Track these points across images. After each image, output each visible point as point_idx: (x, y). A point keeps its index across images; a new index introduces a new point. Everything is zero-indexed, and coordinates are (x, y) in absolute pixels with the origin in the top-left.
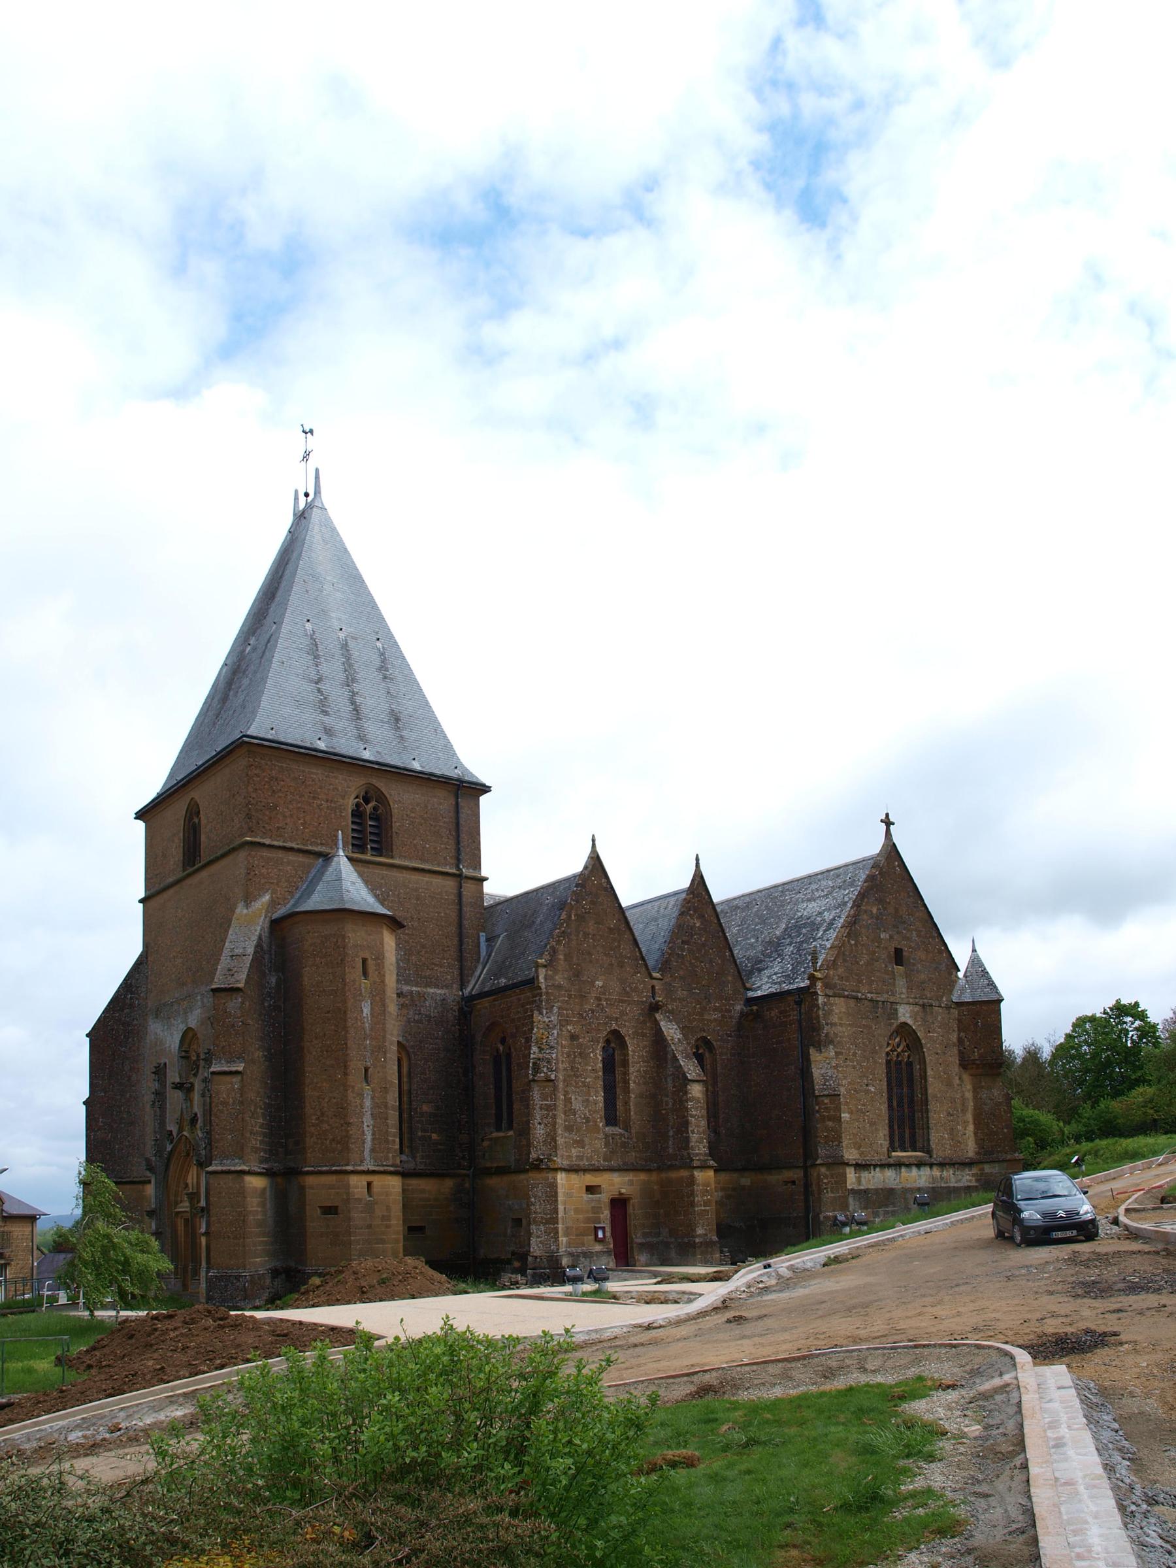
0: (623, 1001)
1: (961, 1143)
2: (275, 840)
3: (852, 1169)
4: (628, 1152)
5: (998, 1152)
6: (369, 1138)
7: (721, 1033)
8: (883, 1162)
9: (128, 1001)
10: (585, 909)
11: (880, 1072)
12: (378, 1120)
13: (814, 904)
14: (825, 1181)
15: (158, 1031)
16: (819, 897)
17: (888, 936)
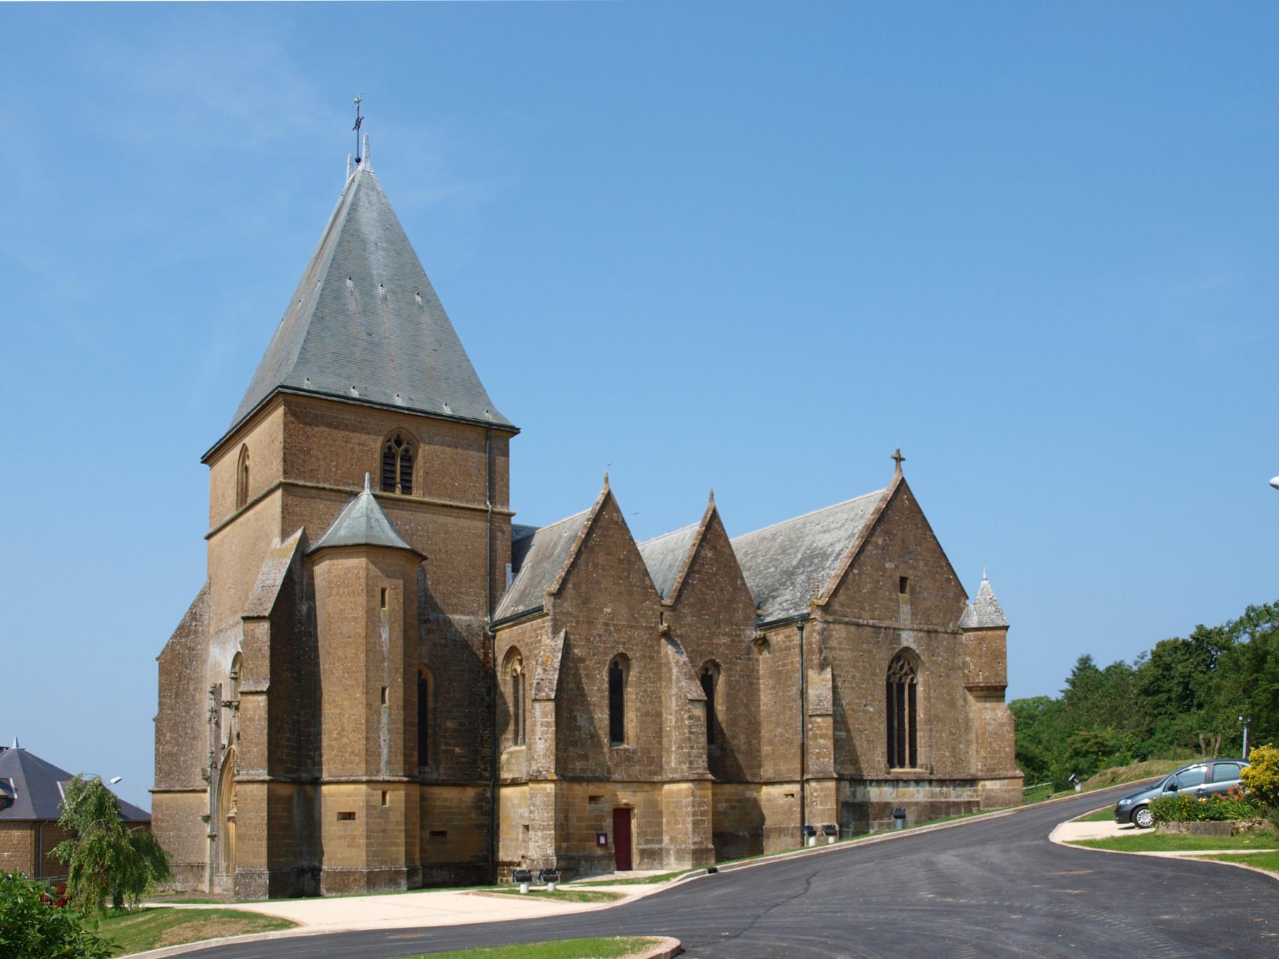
0: (632, 627)
1: (963, 761)
2: (309, 481)
3: (847, 784)
4: (632, 766)
5: (1000, 770)
6: (385, 751)
7: (730, 656)
8: (880, 778)
9: (193, 628)
10: (595, 541)
11: (880, 693)
12: (395, 735)
13: (828, 535)
15: (217, 655)
16: (834, 529)
17: (893, 566)
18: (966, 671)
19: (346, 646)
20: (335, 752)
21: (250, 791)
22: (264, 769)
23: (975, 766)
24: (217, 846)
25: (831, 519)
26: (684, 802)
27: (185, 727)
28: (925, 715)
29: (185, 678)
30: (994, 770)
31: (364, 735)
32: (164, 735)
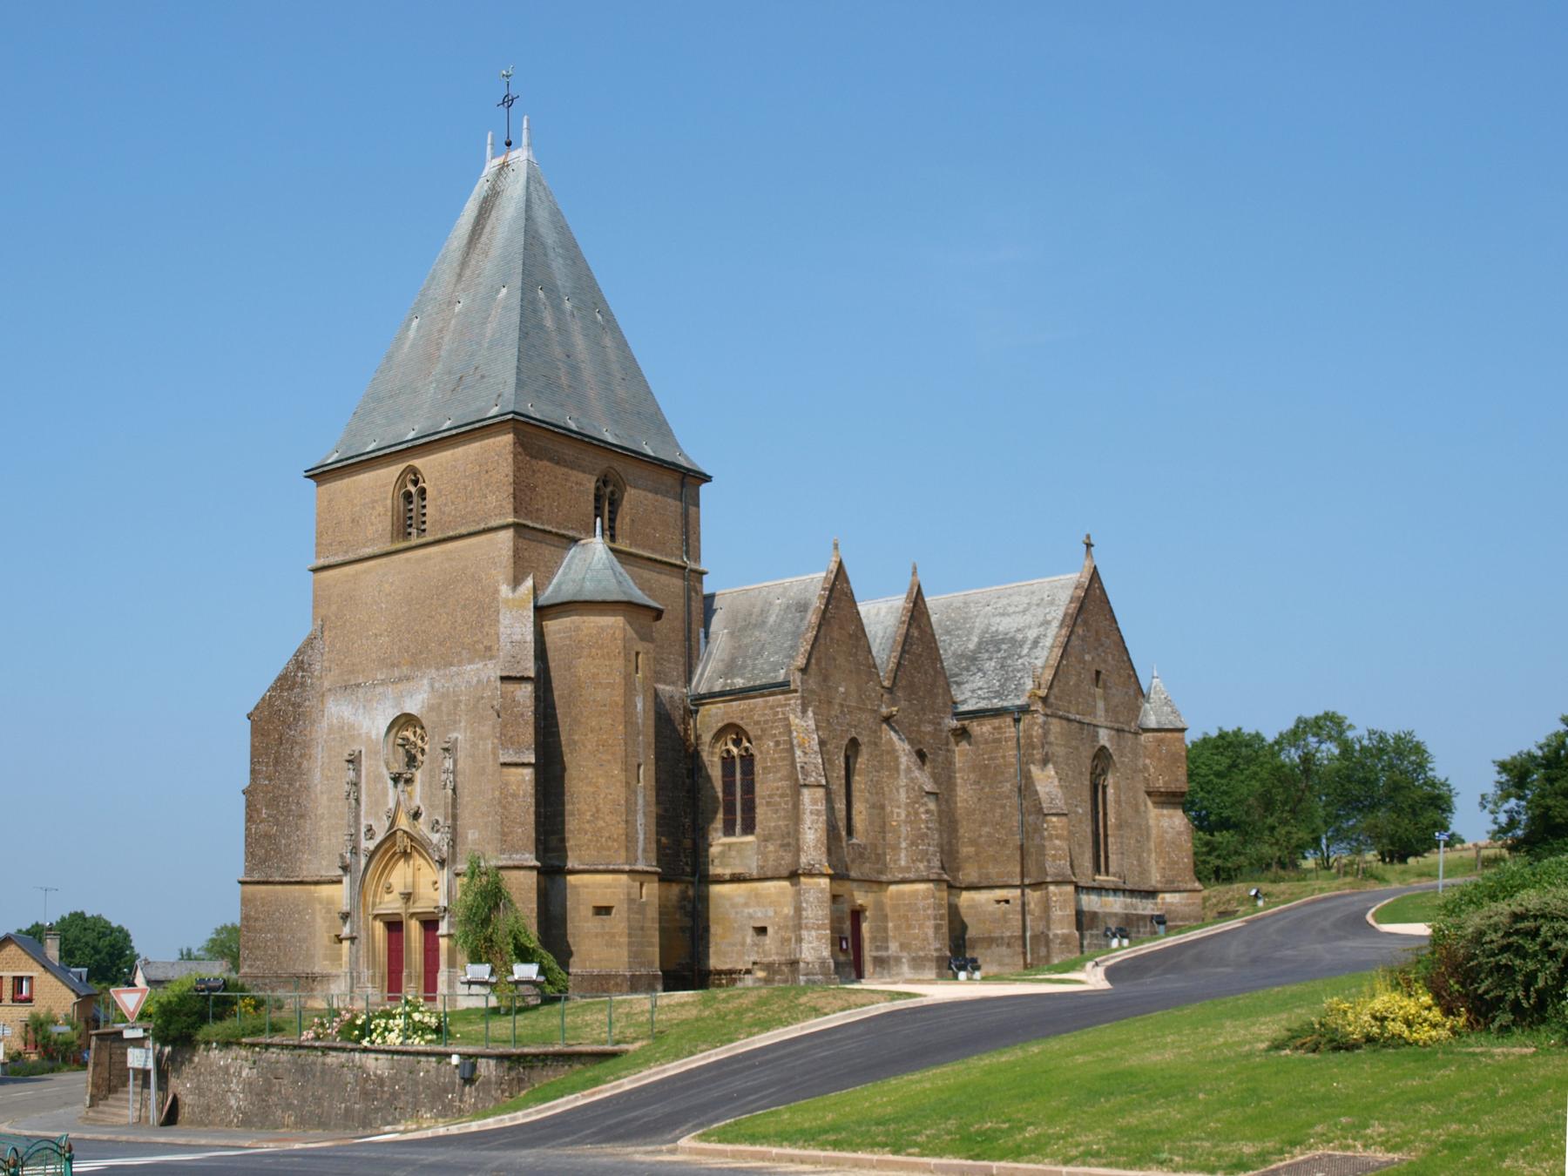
0: (860, 709)
6: (641, 837)
9: (299, 680)
14: (1054, 899)
16: (1014, 613)
18: (1146, 775)
19: (600, 715)
20: (588, 836)
21: (516, 879)
22: (531, 853)
23: (1155, 879)
24: (358, 951)
25: (1004, 601)
26: (921, 904)
27: (288, 802)
28: (1116, 819)
29: (287, 742)
30: (1173, 882)
31: (624, 817)
32: (259, 812)
